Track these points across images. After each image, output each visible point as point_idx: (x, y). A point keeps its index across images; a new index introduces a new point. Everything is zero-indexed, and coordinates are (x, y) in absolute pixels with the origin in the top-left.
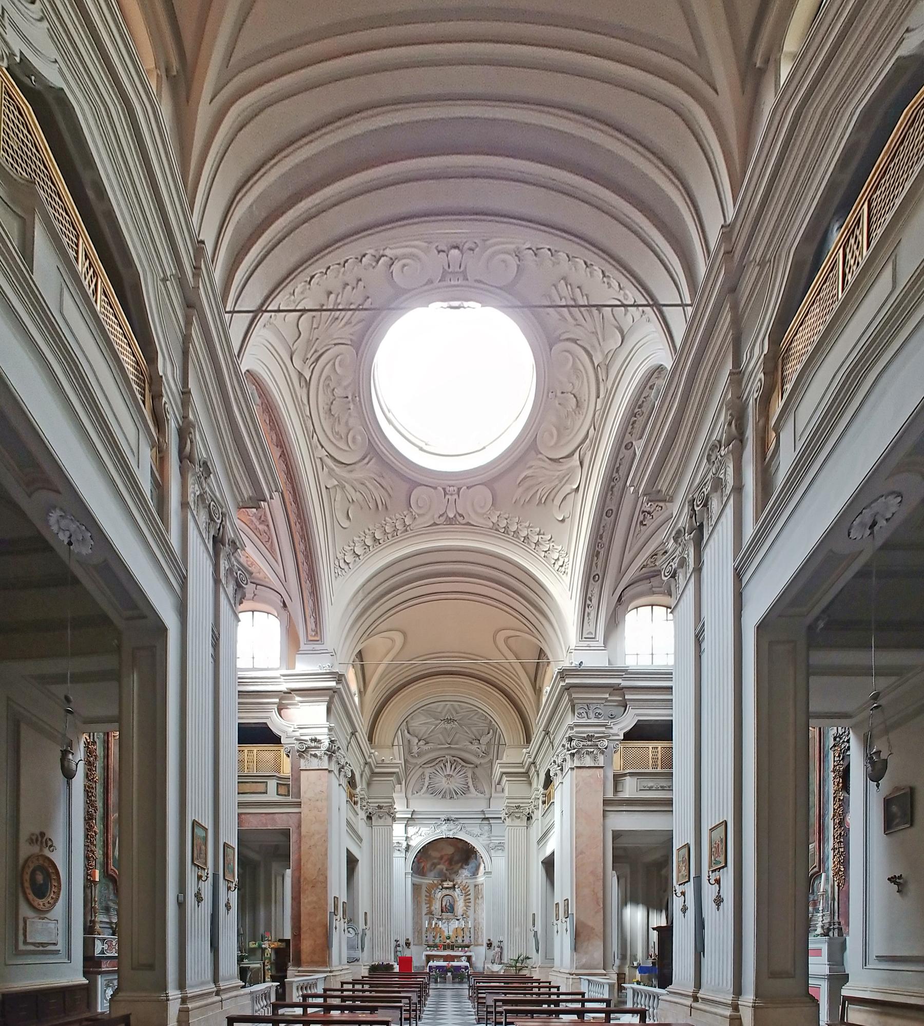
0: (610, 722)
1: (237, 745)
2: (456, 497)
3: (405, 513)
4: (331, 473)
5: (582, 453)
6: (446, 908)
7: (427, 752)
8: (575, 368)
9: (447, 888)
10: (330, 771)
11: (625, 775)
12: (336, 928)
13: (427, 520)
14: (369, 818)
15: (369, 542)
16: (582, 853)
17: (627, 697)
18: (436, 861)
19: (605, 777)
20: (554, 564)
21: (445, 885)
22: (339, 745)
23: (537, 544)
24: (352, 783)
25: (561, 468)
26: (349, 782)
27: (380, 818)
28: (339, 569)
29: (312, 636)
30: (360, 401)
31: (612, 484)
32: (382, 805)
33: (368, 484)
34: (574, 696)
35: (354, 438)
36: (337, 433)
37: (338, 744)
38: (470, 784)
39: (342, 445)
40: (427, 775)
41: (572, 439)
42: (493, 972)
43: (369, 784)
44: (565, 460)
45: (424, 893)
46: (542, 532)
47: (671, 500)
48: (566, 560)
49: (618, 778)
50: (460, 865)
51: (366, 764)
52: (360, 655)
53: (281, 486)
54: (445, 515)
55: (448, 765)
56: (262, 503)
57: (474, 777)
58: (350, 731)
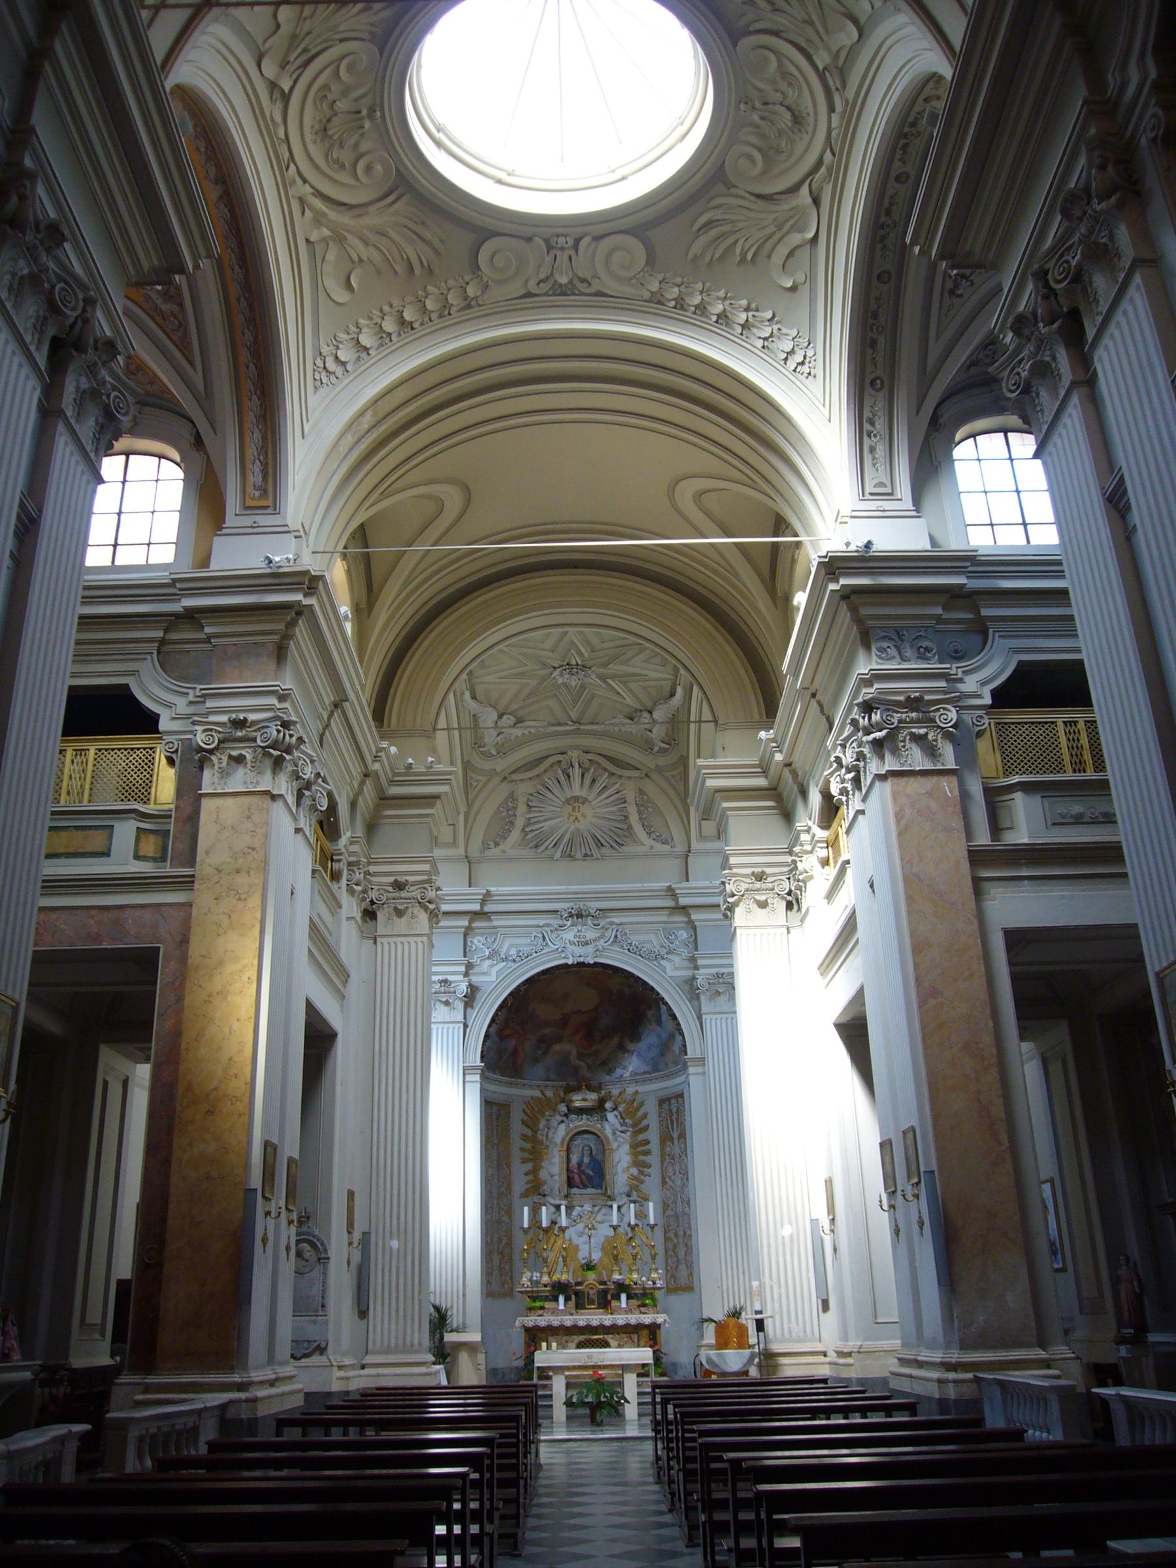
0: (954, 668)
1: (59, 737)
2: (572, 253)
3: (467, 278)
4: (319, 220)
5: (814, 186)
6: (581, 1172)
7: (520, 743)
8: (785, 74)
9: (581, 1111)
10: (274, 797)
11: (1011, 788)
12: (264, 1241)
13: (516, 288)
14: (370, 914)
15: (389, 326)
16: (934, 993)
17: (985, 612)
18: (547, 1031)
19: (965, 796)
20: (786, 359)
21: (578, 1100)
22: (302, 733)
23: (746, 326)
24: (328, 825)
25: (777, 208)
26: (321, 823)
27: (399, 913)
28: (324, 374)
29: (253, 498)
30: (383, 116)
31: (881, 232)
32: (401, 879)
33: (392, 233)
34: (863, 611)
35: (369, 169)
36: (337, 161)
37: (298, 731)
38: (634, 818)
39: (344, 177)
40: (522, 800)
41: (793, 166)
42: (724, 1374)
43: (371, 828)
44: (784, 197)
45: (517, 1128)
46: (753, 306)
47: (995, 266)
48: (810, 353)
49: (994, 796)
50: (615, 1041)
51: (366, 775)
52: (362, 535)
53: (217, 247)
54: (551, 282)
55: (576, 772)
56: (177, 277)
57: (644, 803)
58: (329, 697)
